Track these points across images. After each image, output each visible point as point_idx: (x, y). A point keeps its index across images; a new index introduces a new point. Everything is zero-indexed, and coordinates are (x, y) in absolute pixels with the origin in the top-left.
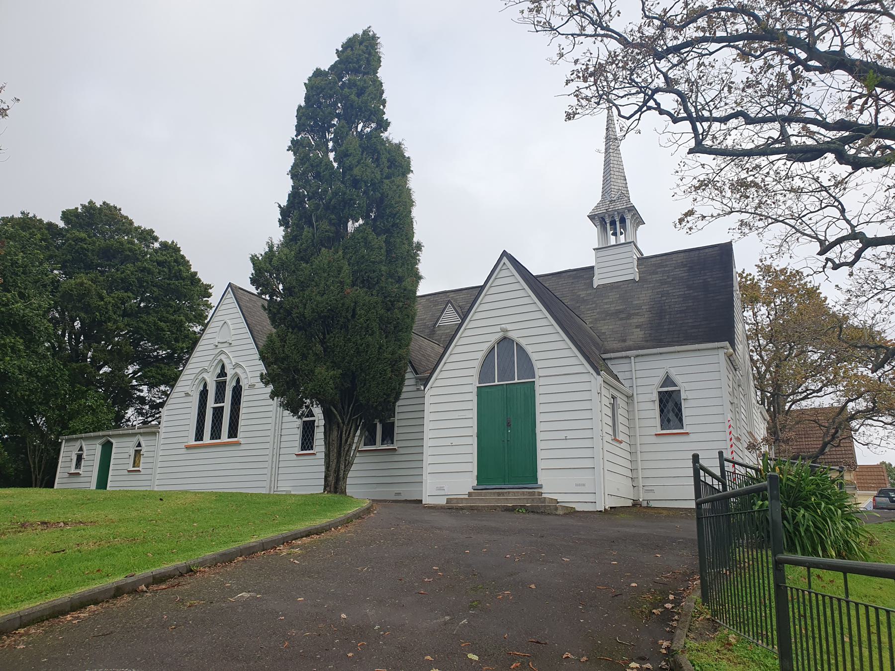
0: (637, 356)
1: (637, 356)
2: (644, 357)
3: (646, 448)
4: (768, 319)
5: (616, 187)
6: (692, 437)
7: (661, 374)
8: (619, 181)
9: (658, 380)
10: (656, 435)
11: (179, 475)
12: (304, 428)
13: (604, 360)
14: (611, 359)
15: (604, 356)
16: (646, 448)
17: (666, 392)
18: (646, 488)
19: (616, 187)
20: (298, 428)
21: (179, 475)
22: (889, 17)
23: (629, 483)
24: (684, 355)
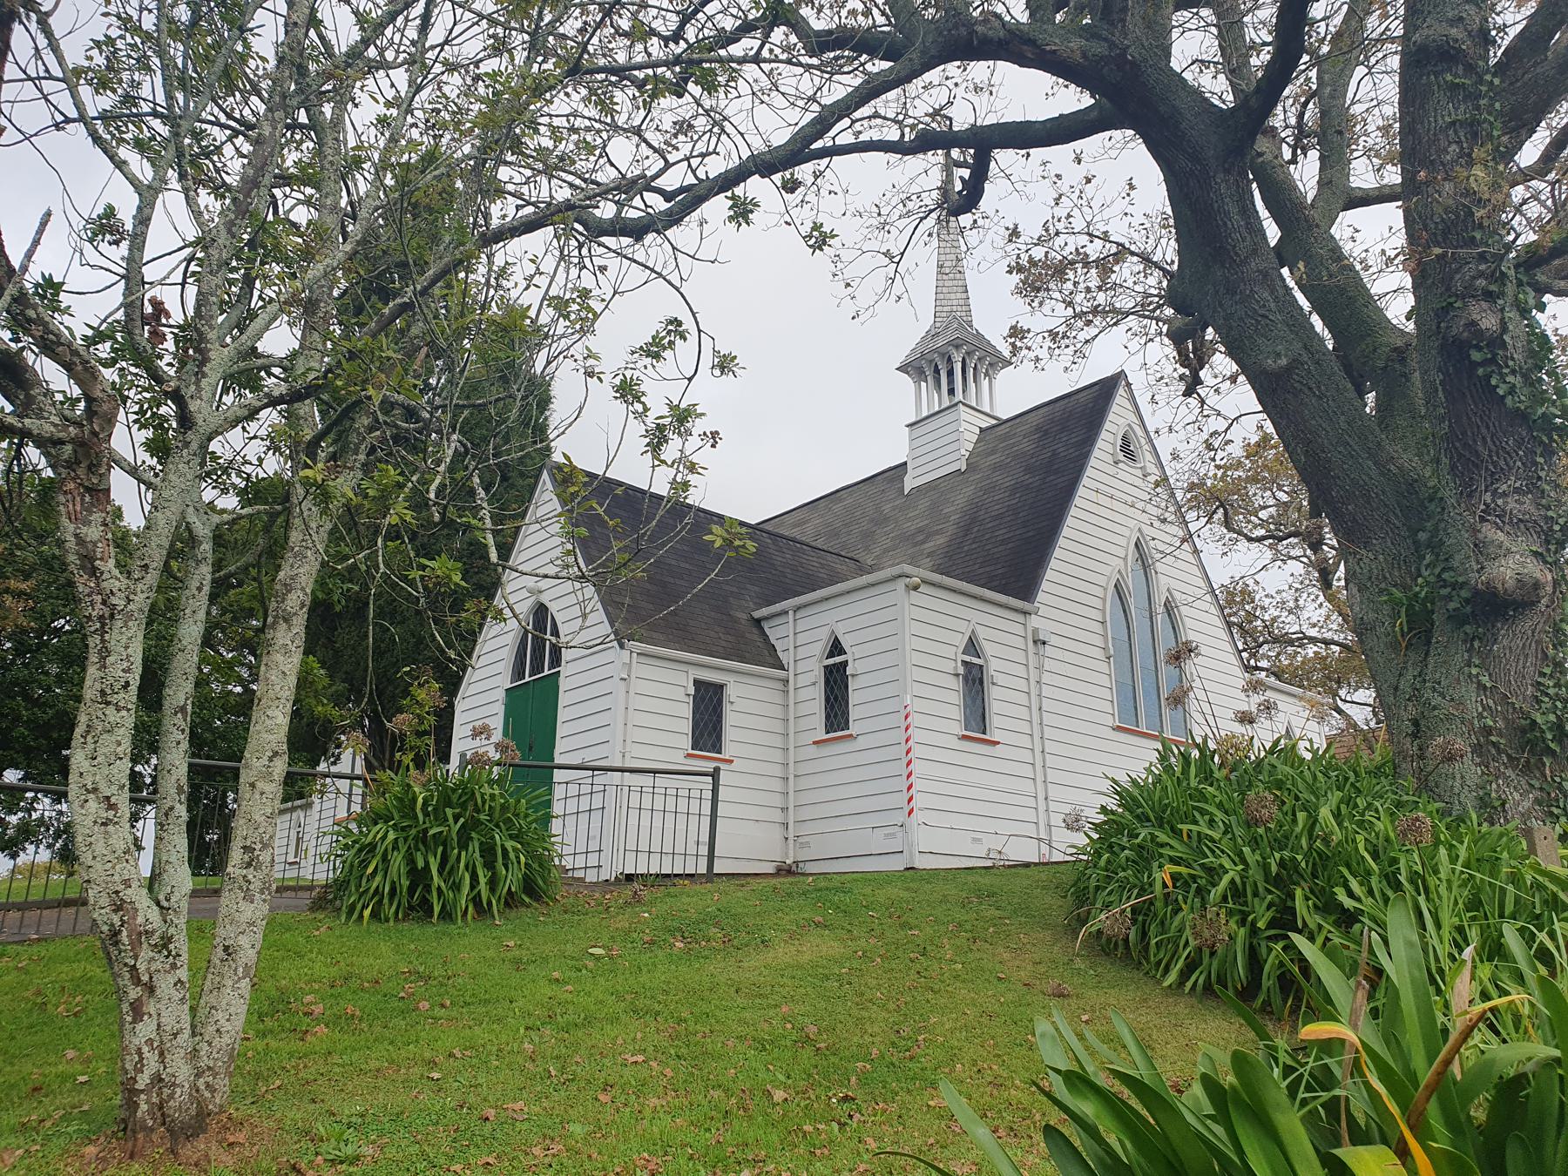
0: (797, 609)
1: (797, 609)
2: (832, 601)
3: (804, 769)
4: (124, 713)
5: (945, 309)
6: (861, 743)
7: (824, 635)
8: (953, 296)
9: (820, 648)
10: (815, 743)
11: (1082, 687)
12: (827, 682)
13: (758, 622)
14: (767, 618)
15: (757, 614)
16: (804, 769)
17: (834, 665)
18: (800, 840)
19: (945, 309)
20: (814, 684)
21: (1082, 687)
22: (1023, 62)
23: (778, 832)
24: (832, 604)
